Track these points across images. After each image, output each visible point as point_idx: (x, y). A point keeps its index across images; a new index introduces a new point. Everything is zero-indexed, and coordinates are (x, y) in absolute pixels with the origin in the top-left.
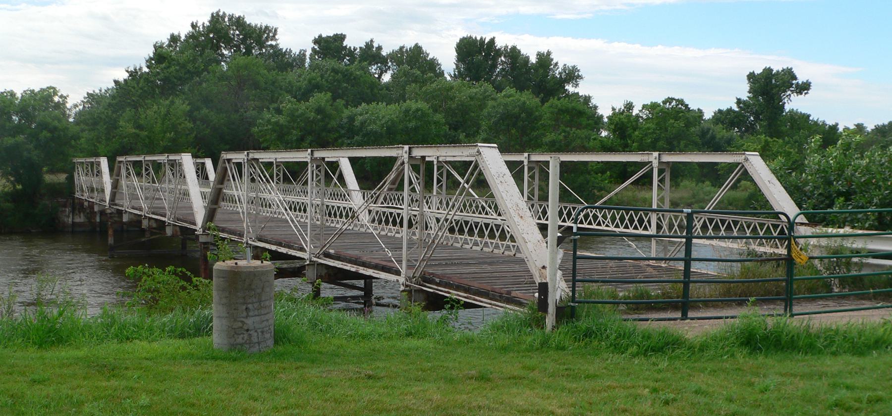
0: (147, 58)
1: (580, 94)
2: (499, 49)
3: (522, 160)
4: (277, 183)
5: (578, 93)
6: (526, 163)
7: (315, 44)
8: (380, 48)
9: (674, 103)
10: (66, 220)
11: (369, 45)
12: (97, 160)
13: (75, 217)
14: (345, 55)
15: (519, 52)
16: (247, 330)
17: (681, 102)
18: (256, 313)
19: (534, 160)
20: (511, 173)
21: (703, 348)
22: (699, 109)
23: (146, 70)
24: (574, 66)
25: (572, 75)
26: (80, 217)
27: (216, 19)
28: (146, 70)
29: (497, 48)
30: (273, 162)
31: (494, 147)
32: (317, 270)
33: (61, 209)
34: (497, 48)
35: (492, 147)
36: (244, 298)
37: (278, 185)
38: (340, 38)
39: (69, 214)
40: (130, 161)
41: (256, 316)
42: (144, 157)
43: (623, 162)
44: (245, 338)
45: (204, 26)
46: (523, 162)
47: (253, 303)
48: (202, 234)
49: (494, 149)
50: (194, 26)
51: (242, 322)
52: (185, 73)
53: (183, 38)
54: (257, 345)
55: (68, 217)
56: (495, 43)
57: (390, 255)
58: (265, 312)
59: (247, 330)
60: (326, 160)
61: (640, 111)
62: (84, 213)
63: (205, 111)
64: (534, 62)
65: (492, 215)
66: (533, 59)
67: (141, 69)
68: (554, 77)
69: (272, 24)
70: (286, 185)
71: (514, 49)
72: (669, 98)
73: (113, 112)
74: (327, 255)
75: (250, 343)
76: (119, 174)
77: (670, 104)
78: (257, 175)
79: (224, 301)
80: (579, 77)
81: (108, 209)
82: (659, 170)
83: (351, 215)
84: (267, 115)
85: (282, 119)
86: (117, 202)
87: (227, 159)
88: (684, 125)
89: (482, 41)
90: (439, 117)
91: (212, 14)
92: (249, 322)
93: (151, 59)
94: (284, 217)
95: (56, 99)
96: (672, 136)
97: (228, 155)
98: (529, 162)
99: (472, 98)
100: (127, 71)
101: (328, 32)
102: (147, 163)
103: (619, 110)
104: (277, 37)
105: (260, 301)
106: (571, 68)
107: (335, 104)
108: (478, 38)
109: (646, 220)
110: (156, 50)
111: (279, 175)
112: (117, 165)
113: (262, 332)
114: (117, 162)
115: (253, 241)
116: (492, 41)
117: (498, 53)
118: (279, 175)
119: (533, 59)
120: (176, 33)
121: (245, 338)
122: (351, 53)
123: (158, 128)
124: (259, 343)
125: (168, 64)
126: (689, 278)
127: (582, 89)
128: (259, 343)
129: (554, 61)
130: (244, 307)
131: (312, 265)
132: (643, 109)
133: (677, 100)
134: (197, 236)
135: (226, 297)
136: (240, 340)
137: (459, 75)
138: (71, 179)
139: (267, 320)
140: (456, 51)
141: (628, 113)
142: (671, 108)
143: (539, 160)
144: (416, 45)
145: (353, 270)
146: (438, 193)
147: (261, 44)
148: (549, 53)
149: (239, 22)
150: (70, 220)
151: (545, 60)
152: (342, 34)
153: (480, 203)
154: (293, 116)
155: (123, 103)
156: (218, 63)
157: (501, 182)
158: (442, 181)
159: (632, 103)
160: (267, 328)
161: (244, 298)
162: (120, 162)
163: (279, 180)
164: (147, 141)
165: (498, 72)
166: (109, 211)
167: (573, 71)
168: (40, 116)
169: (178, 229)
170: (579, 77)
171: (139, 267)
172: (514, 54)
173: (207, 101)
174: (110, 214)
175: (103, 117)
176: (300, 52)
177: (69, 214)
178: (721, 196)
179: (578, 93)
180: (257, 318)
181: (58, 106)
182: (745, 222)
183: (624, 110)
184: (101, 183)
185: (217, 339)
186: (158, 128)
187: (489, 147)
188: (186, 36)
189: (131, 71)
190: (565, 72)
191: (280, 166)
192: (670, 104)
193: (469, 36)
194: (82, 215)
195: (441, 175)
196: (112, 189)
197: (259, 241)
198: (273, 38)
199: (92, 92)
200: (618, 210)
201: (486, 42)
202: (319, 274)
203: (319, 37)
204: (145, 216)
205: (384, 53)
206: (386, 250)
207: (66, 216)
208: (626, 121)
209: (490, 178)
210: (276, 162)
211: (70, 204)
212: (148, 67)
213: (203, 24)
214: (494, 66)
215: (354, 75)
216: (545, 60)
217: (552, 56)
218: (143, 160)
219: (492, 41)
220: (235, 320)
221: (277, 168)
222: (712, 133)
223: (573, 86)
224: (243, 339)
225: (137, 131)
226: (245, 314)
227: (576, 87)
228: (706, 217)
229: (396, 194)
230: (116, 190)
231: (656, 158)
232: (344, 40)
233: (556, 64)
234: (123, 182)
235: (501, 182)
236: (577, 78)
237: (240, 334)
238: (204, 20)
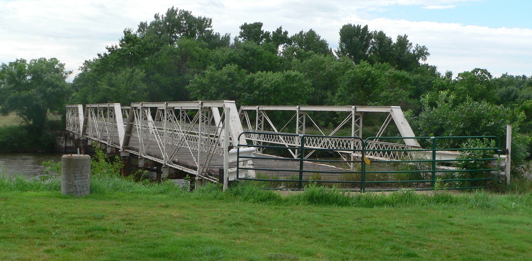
0: (121, 39)
1: (429, 65)
2: (371, 34)
5: (427, 64)
6: (353, 113)
7: (241, 29)
8: (286, 33)
9: (479, 72)
10: (61, 145)
11: (279, 31)
12: (110, 106)
13: (67, 143)
14: (262, 37)
15: (385, 35)
16: (75, 186)
17: (484, 71)
18: (80, 178)
21: (287, 200)
22: (524, 76)
23: (119, 47)
24: (424, 46)
25: (422, 52)
26: (70, 143)
27: (171, 13)
28: (119, 47)
29: (369, 33)
30: (179, 110)
31: (233, 103)
32: (169, 171)
33: (58, 137)
34: (369, 33)
35: (232, 102)
36: (74, 171)
38: (259, 25)
39: (63, 141)
40: (93, 107)
41: (79, 179)
42: (167, 104)
43: (328, 111)
44: (74, 189)
45: (162, 18)
46: (351, 112)
47: (78, 173)
49: (233, 104)
50: (156, 17)
51: (72, 182)
52: (145, 50)
53: (148, 24)
54: (79, 193)
55: (63, 142)
56: (367, 29)
57: (195, 161)
58: (85, 178)
59: (75, 186)
60: (175, 108)
61: (457, 78)
62: (73, 140)
63: (157, 75)
64: (396, 43)
65: (282, 142)
66: (395, 41)
67: (116, 47)
68: (408, 52)
69: (208, 16)
70: (187, 124)
71: (381, 33)
72: (476, 69)
73: (98, 75)
74: (174, 162)
75: (77, 192)
76: (88, 116)
77: (477, 73)
78: (173, 119)
79: (65, 172)
80: (428, 54)
81: (81, 137)
82: (355, 116)
84: (196, 77)
85: (205, 81)
86: (87, 133)
87: (134, 107)
88: (485, 88)
89: (359, 27)
90: (308, 82)
91: (169, 9)
92: (76, 182)
93: (123, 40)
95: (56, 66)
96: (477, 95)
98: (355, 112)
99: (337, 68)
100: (107, 48)
101: (250, 21)
102: (100, 108)
103: (442, 77)
104: (211, 25)
105: (81, 173)
106: (422, 47)
107: (240, 72)
108: (356, 26)
109: (349, 145)
110: (125, 35)
112: (86, 109)
113: (83, 187)
114: (86, 108)
115: (144, 155)
116: (366, 28)
117: (370, 36)
119: (395, 41)
120: (144, 21)
121: (74, 189)
122: (267, 34)
123: (123, 86)
124: (81, 192)
125: (132, 44)
126: (302, 170)
127: (430, 61)
128: (81, 192)
129: (410, 42)
130: (74, 175)
132: (459, 76)
133: (482, 70)
134: (120, 152)
135: (66, 171)
136: (71, 190)
137: (342, 53)
138: (64, 118)
139: (85, 182)
140: (340, 34)
141: (448, 79)
142: (478, 76)
143: (304, 110)
144: (311, 30)
145: (181, 169)
147: (202, 30)
148: (406, 37)
149: (186, 15)
150: (64, 145)
151: (403, 42)
152: (260, 23)
154: (212, 78)
155: (104, 69)
156: (172, 42)
157: (232, 121)
158: (359, 128)
159: (452, 72)
160: (85, 186)
161: (74, 171)
162: (88, 108)
163: (260, 126)
164: (115, 94)
165: (370, 49)
166: (82, 139)
167: (423, 50)
168: (47, 77)
169: (114, 149)
170: (428, 54)
171: (49, 162)
172: (381, 37)
173: (159, 68)
174: (83, 140)
175: (91, 78)
176: (225, 36)
177: (63, 141)
179: (427, 64)
180: (80, 181)
181: (57, 71)
182: (391, 146)
183: (445, 77)
184: (78, 120)
185: (63, 191)
186: (123, 86)
187: (230, 102)
188: (150, 24)
189: (110, 48)
190: (417, 50)
191: (184, 112)
192: (477, 73)
193: (349, 24)
194: (71, 141)
195: (302, 120)
196: (84, 124)
197: (148, 155)
198: (209, 26)
199: (88, 61)
200: (311, 137)
201: (361, 28)
202: (170, 173)
203: (245, 24)
205: (289, 36)
206: (194, 158)
207: (61, 142)
208: (446, 84)
209: (398, 124)
211: (64, 134)
212: (121, 46)
213: (163, 16)
214: (367, 46)
215: (257, 52)
216: (403, 42)
217: (408, 39)
218: (98, 107)
219: (366, 28)
220: (69, 181)
221: (355, 120)
222: (515, 93)
223: (422, 60)
224: (73, 190)
225: (109, 87)
226: (74, 178)
227: (424, 61)
228: (390, 145)
230: (86, 126)
231: (353, 109)
232: (261, 27)
233: (411, 44)
234: (138, 123)
235: (232, 121)
236: (425, 54)
237: (71, 188)
238: (163, 13)
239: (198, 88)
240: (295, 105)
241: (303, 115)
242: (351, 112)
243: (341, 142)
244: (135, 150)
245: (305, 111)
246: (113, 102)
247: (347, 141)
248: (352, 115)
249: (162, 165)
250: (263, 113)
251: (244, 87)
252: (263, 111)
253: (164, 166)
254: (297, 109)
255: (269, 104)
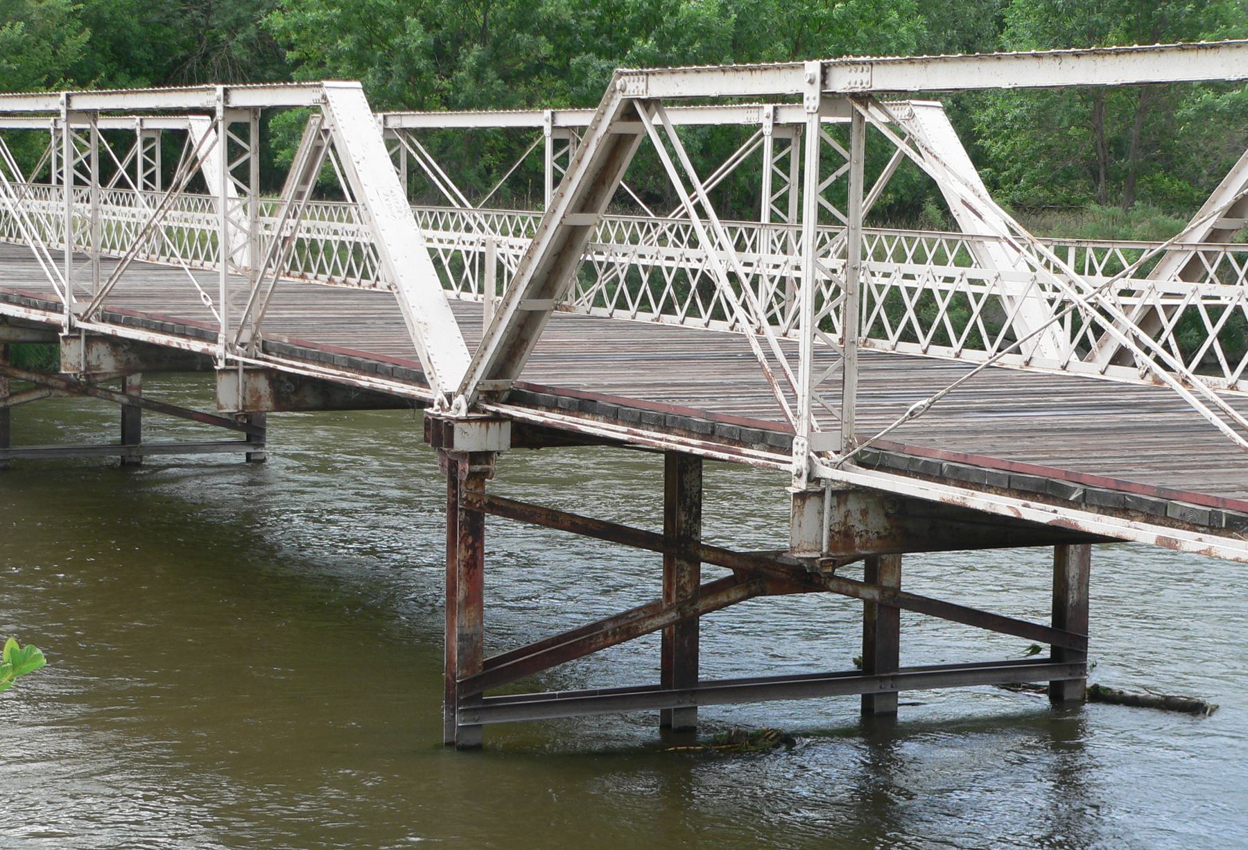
3: (541, 124)
4: (146, 187)
6: (767, 129)
19: (563, 124)
20: (389, 150)
37: (149, 194)
43: (439, 129)
46: (760, 126)
48: (468, 420)
83: (207, 245)
94: (20, 241)
97: (877, 70)
111: (151, 166)
118: (151, 166)
131: (815, 494)
146: (774, 218)
153: (463, 219)
163: (151, 178)
169: (262, 384)
178: (434, 179)
204: (72, 329)
210: (142, 130)
221: (555, 151)
229: (523, 219)
231: (768, 117)
239: (344, 30)
240: (530, 103)
241: (153, 140)
242: (760, 126)
243: (431, 217)
244: (273, 349)
245: (573, 128)
246: (324, 69)
247: (518, 218)
248: (762, 135)
249: (57, 328)
250: (403, 137)
251: (578, 22)
252: (403, 131)
253: (66, 332)
254: (547, 120)
255: (419, 106)
